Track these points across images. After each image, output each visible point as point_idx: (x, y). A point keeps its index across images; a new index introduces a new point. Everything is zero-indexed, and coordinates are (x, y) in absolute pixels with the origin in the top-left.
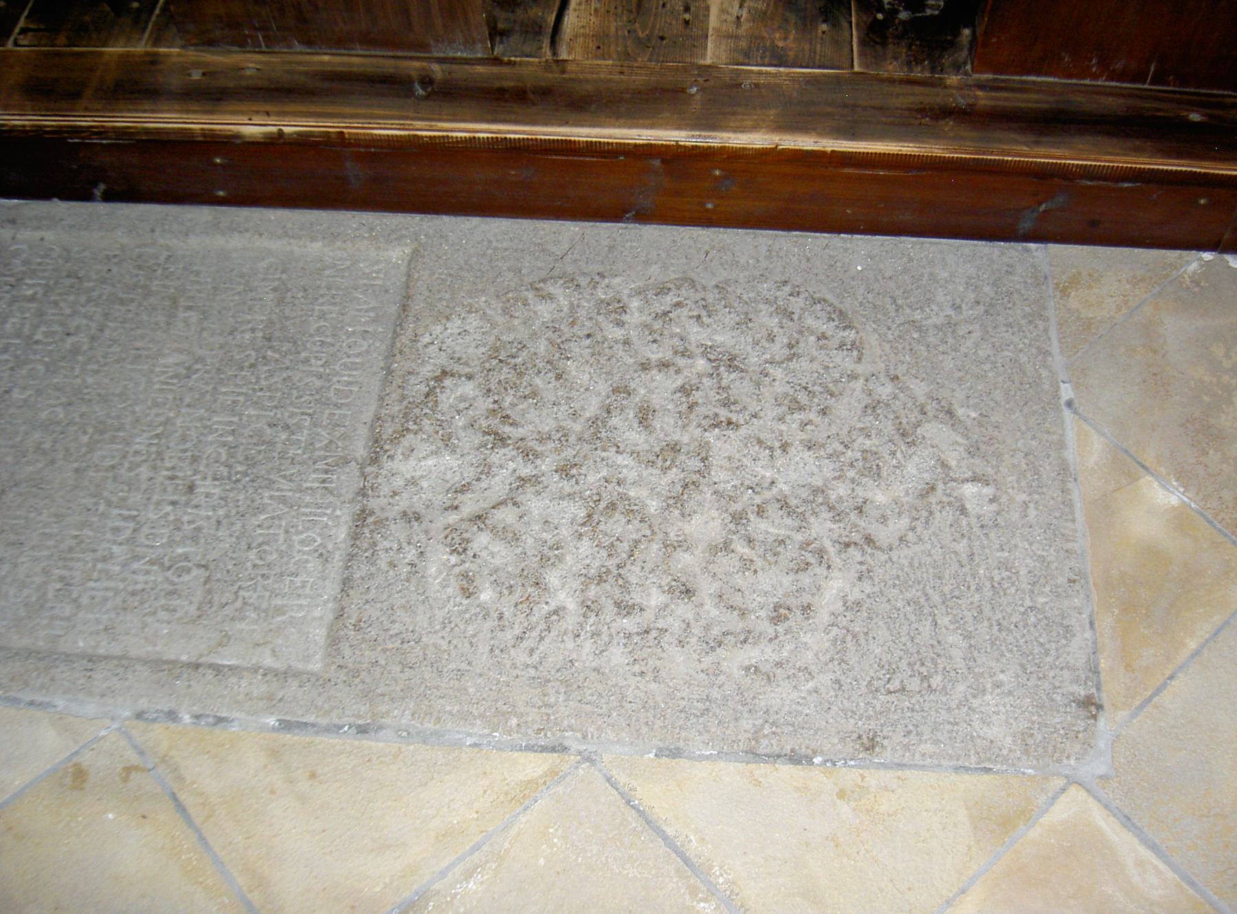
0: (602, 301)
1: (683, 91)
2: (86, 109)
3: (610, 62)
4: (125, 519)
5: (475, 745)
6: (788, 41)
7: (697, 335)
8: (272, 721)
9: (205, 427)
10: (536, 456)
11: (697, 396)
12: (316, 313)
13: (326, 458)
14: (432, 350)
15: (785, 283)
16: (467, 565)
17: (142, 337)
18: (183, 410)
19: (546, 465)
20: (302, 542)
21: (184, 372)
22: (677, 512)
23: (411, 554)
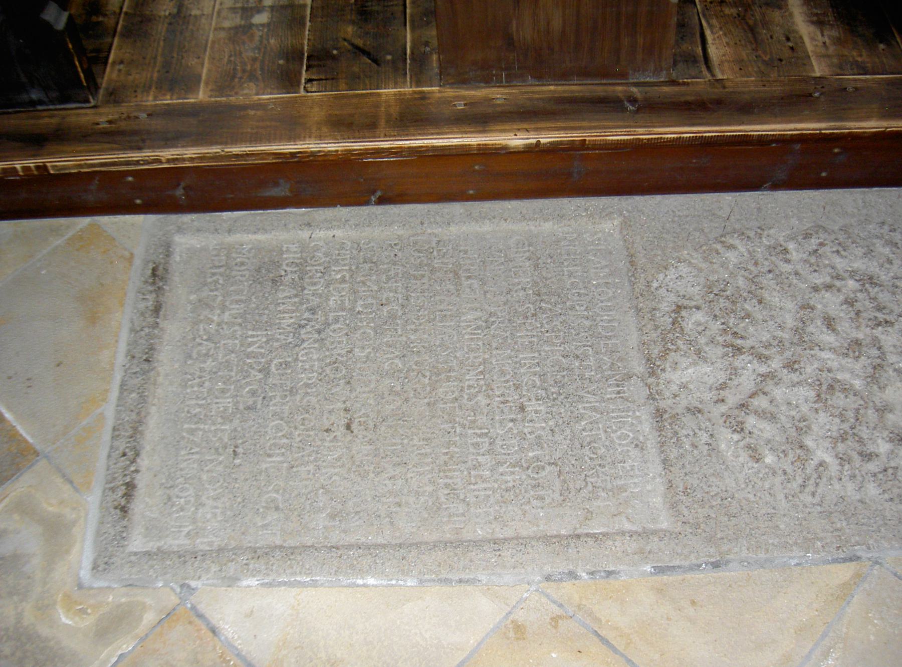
0: (770, 246)
1: (810, 95)
2: (385, 136)
3: (753, 79)
4: (480, 436)
5: (798, 564)
6: (863, 57)
7: (840, 263)
8: (648, 568)
9: (516, 363)
10: (767, 358)
11: (858, 305)
12: (566, 273)
13: (614, 376)
14: (662, 291)
15: (883, 223)
16: (748, 439)
17: (441, 302)
18: (494, 352)
19: (776, 364)
20: (619, 438)
21: (484, 324)
22: (875, 387)
23: (704, 437)
